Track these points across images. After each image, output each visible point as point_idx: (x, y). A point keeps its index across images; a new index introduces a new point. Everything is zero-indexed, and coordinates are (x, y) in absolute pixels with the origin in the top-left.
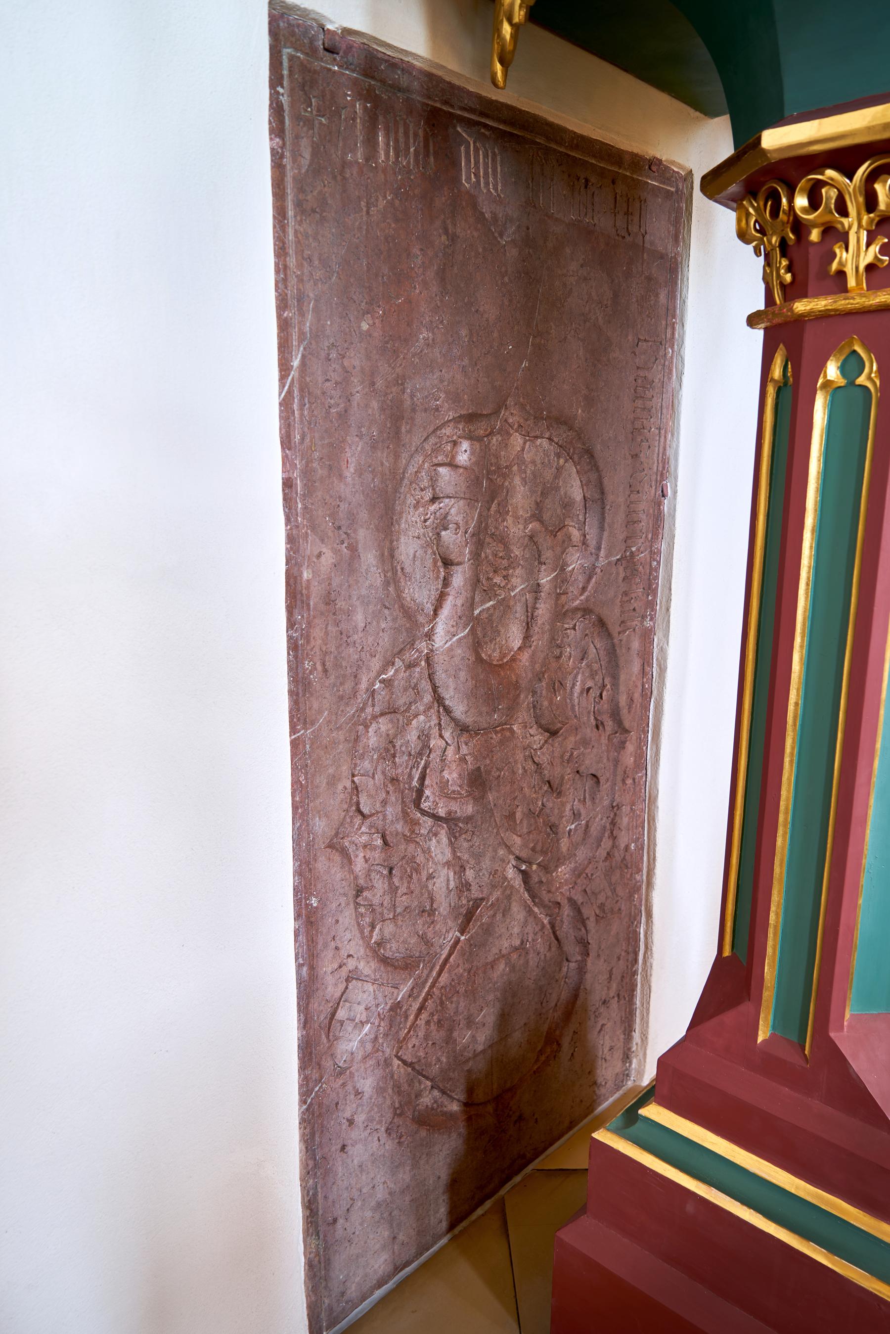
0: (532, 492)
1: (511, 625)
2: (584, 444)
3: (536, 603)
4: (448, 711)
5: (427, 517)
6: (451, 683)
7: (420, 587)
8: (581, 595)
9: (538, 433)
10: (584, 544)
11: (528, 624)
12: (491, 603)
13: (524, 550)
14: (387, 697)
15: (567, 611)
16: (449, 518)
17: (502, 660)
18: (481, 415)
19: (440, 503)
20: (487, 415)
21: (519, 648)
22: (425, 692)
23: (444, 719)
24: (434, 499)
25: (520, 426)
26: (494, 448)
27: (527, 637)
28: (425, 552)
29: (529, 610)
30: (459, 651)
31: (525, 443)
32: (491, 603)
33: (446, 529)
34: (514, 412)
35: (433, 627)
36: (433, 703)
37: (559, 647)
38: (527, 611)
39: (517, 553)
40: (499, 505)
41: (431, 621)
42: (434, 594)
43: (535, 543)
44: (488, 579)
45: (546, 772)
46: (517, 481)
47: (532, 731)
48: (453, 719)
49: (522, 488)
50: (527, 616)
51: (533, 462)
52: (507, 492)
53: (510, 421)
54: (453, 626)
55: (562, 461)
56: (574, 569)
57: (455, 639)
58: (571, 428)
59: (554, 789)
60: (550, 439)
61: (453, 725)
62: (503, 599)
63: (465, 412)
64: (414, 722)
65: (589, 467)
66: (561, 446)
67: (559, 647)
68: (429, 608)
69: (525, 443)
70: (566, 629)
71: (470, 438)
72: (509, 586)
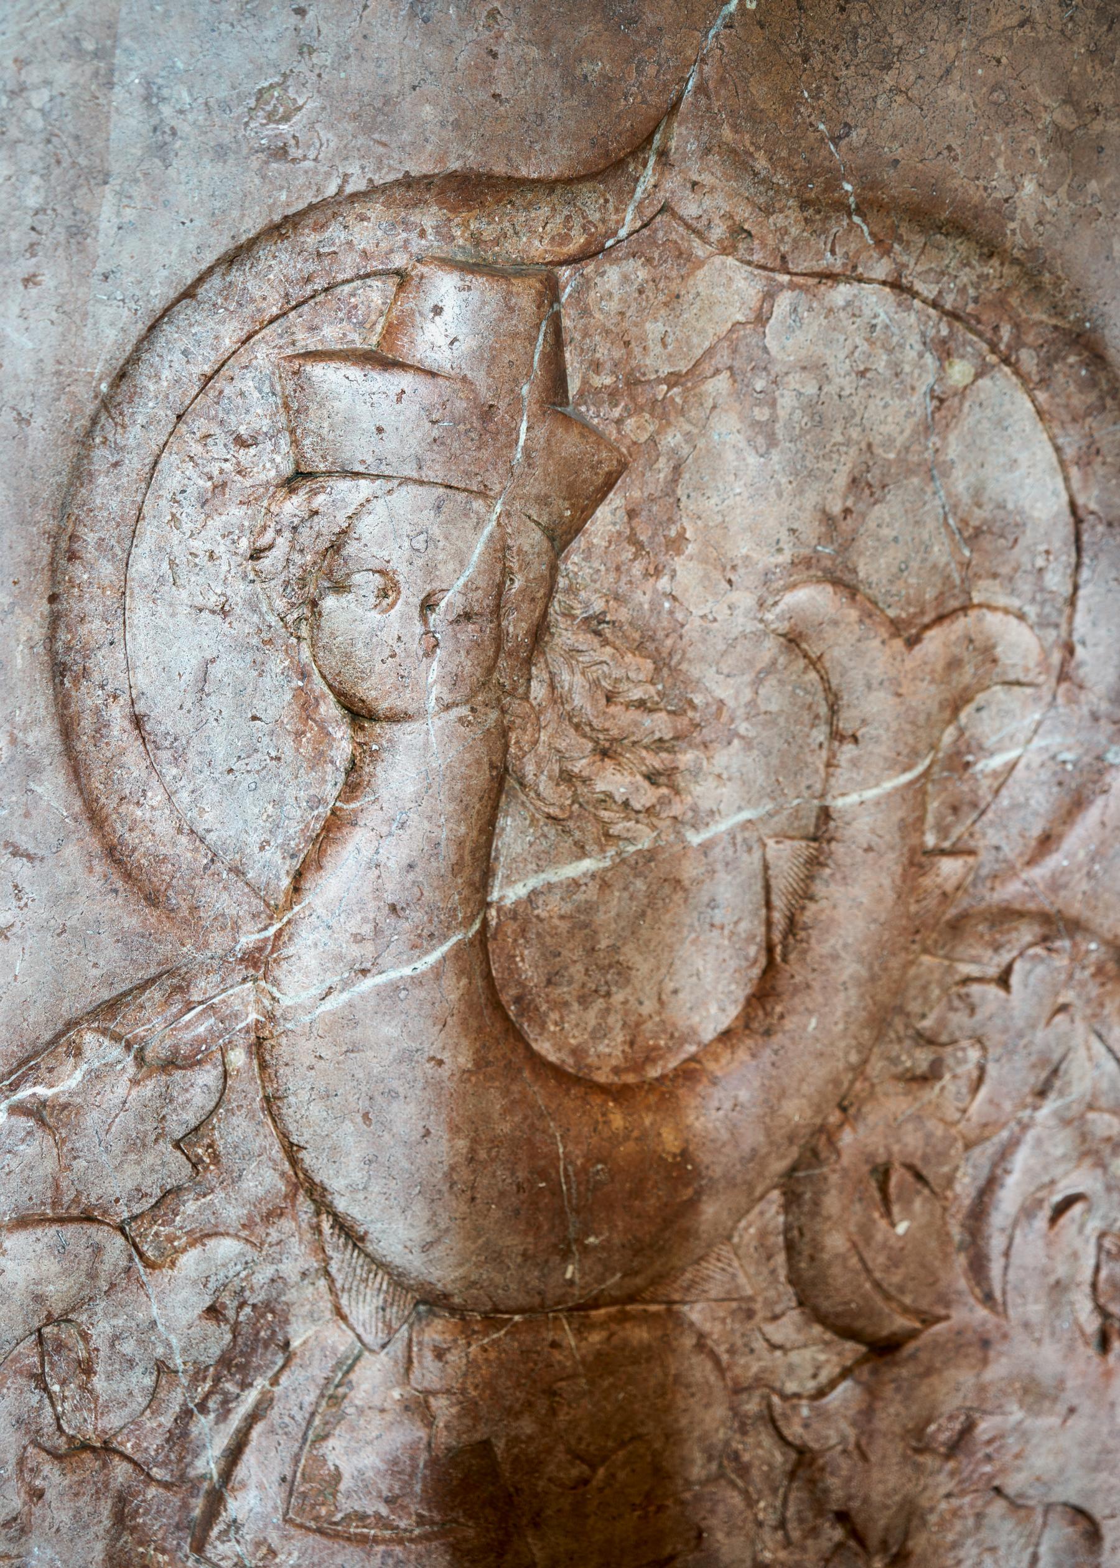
0: (803, 475)
1: (686, 950)
2: (1057, 310)
3: (811, 878)
4: (351, 1234)
5: (264, 541)
6: (350, 1137)
7: (230, 787)
8: (1031, 862)
9: (836, 263)
10: (1063, 676)
11: (770, 949)
12: (587, 865)
13: (758, 682)
14: (49, 1166)
15: (964, 916)
16: (351, 549)
17: (637, 1067)
18: (514, 185)
19: (314, 493)
20: (549, 185)
21: (726, 1036)
22: (248, 1156)
23: (340, 1259)
24: (299, 478)
25: (738, 232)
26: (613, 306)
27: (766, 994)
28: (260, 668)
29: (778, 901)
30: (390, 1030)
31: (769, 296)
32: (587, 865)
33: (340, 588)
34: (706, 179)
35: (278, 935)
36: (292, 1197)
37: (927, 1040)
38: (768, 905)
39: (720, 693)
40: (632, 514)
41: (274, 911)
42: (298, 822)
43: (814, 663)
44: (567, 777)
45: (832, 1482)
46: (728, 431)
47: (780, 1332)
48: (378, 1264)
49: (753, 460)
50: (769, 924)
51: (815, 368)
52: (677, 470)
53: (690, 209)
54: (358, 939)
55: (960, 371)
56: (1012, 766)
57: (367, 984)
58: (990, 249)
59: (873, 1540)
60: (896, 285)
61: (381, 1280)
62: (650, 856)
63: (428, 168)
64: (189, 1261)
65: (1092, 397)
66: (954, 315)
67: (927, 1040)
68: (273, 868)
69: (769, 296)
70: (967, 980)
71: (474, 266)
72: (677, 809)
